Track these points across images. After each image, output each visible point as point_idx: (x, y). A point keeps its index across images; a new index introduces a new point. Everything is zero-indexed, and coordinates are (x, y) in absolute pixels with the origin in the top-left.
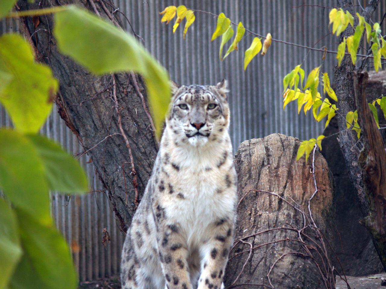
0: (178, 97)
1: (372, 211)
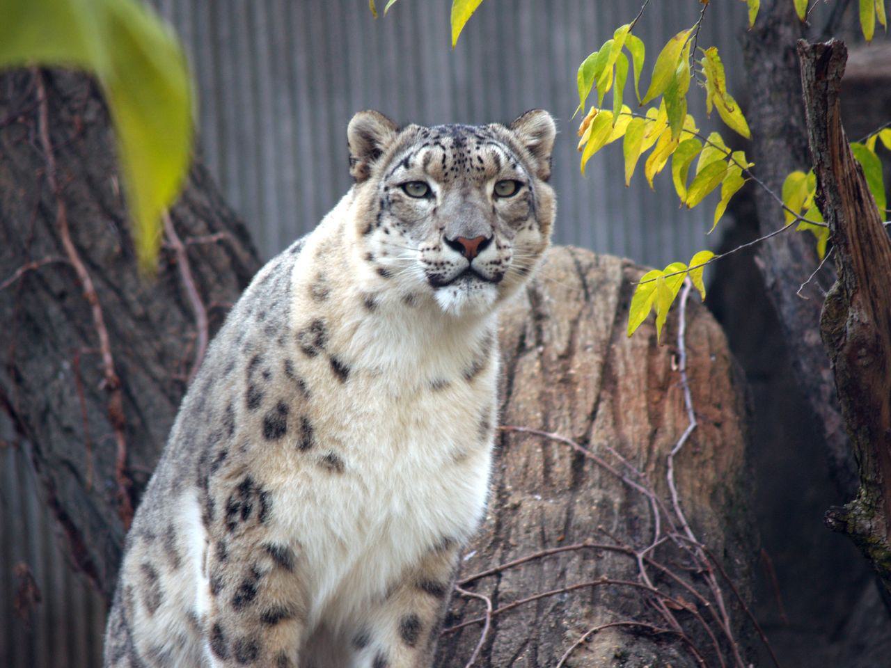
0: (398, 160)
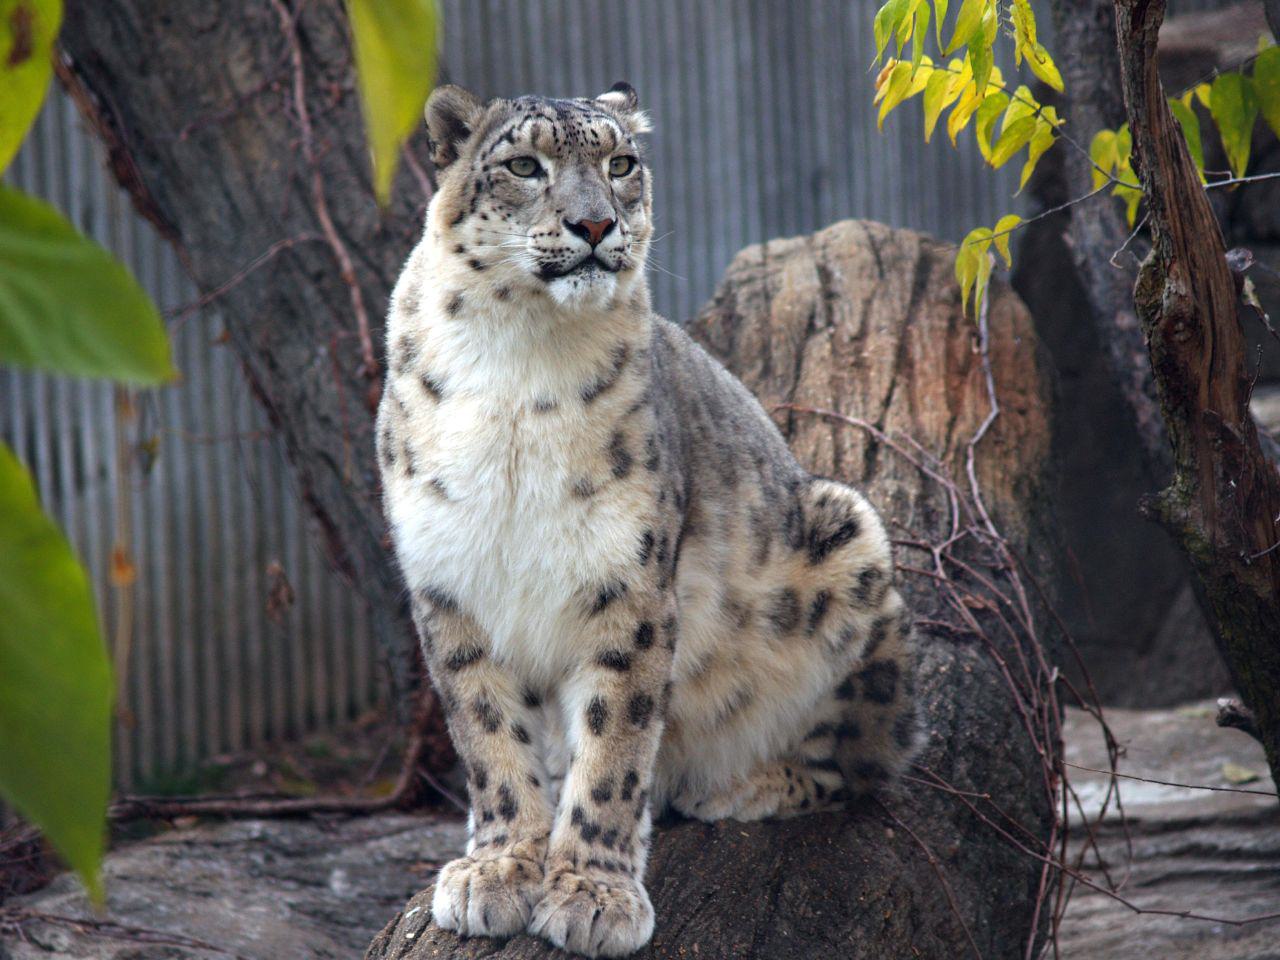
1: (1186, 470)
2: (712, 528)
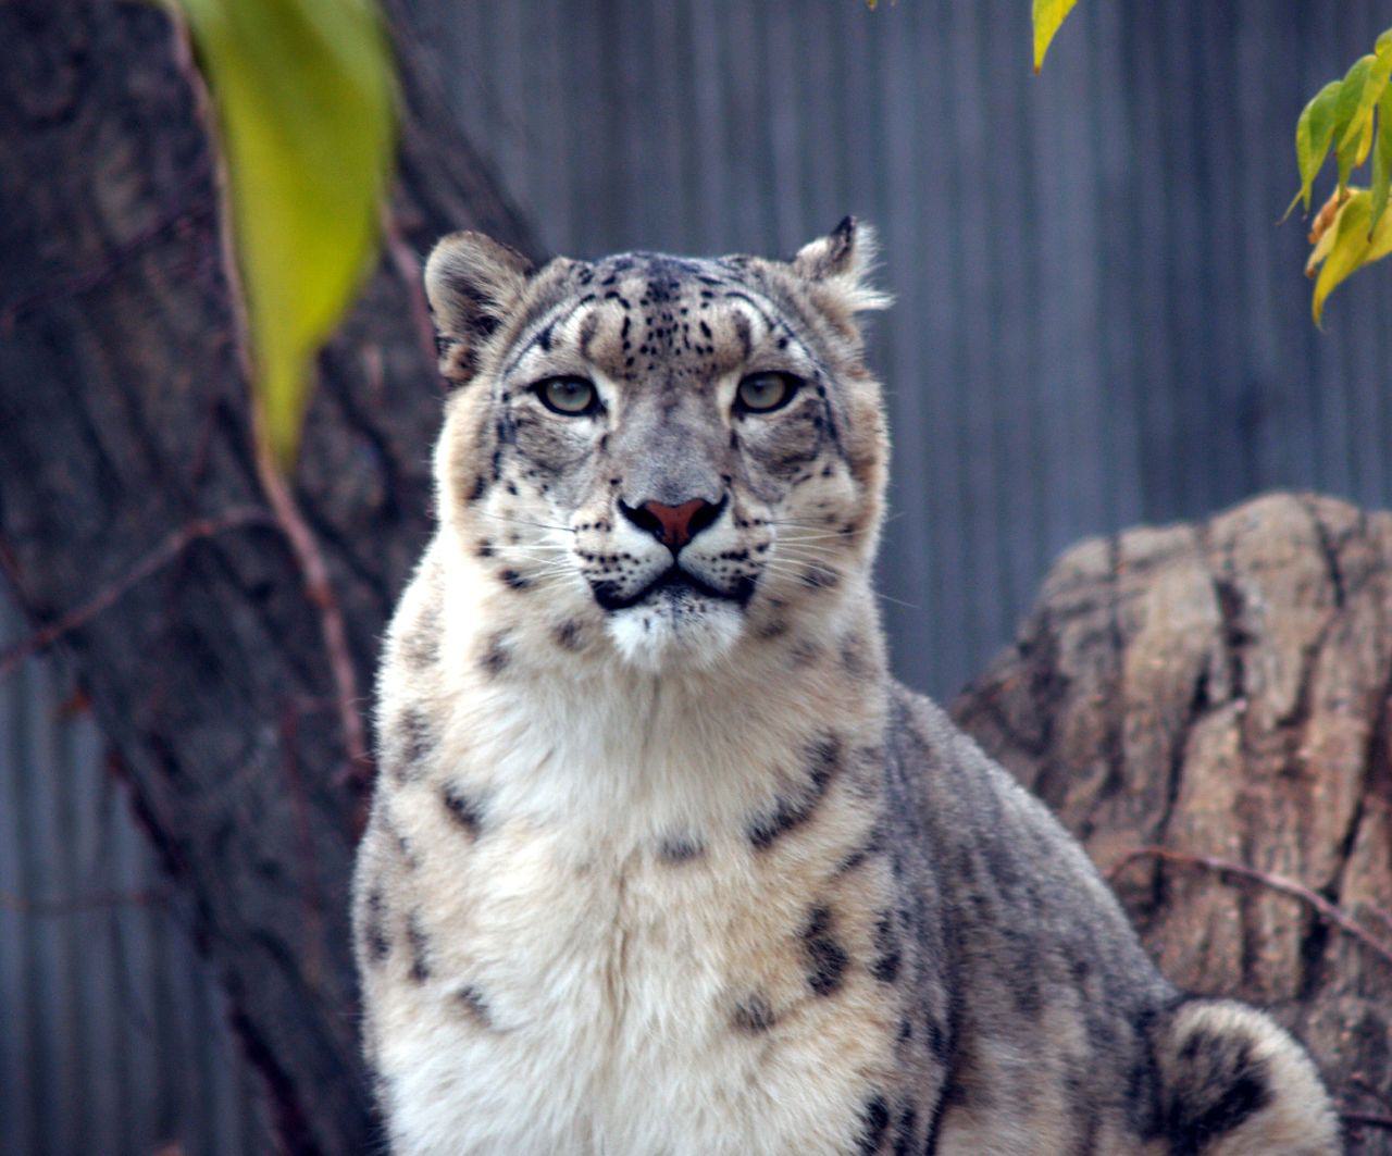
0: (531, 333)
2: (997, 1094)
